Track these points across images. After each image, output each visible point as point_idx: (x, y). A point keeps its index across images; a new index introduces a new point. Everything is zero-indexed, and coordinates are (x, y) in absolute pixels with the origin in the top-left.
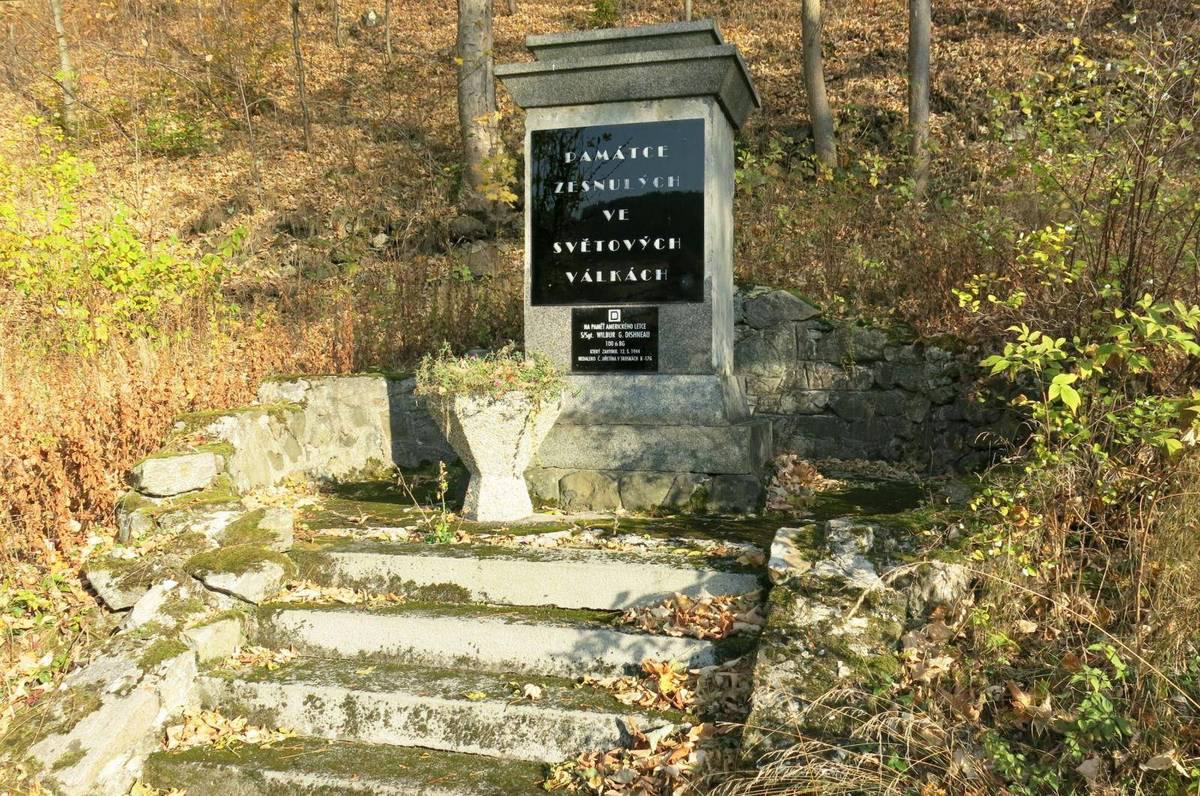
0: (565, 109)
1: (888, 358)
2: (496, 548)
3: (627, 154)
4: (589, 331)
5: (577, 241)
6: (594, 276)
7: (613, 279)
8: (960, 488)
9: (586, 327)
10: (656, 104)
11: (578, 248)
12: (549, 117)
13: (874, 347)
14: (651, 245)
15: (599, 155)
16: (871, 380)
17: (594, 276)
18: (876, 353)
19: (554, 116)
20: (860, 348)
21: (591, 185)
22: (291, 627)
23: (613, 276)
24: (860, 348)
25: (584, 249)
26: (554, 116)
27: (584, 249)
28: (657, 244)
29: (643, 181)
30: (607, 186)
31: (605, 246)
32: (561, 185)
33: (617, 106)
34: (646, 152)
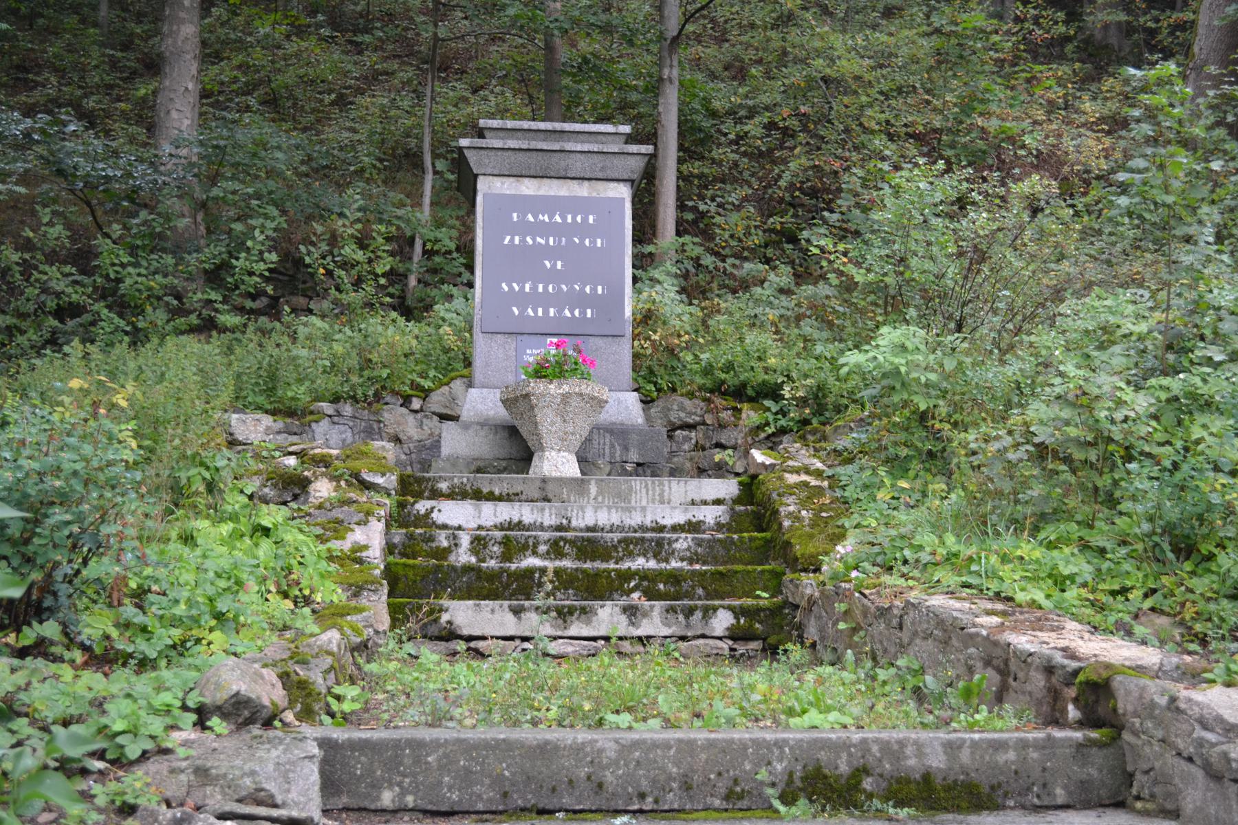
0: (512, 179)
1: (709, 422)
2: (355, 608)
3: (564, 218)
4: (531, 355)
5: (522, 283)
6: (535, 312)
7: (552, 314)
8: (808, 241)
9: (529, 352)
10: (586, 183)
11: (522, 288)
12: (499, 184)
13: (695, 414)
14: (583, 290)
15: (541, 217)
16: (693, 441)
17: (535, 312)
18: (698, 419)
19: (503, 184)
20: (682, 415)
21: (534, 240)
22: (423, 512)
23: (552, 312)
24: (682, 415)
25: (527, 290)
26: (503, 184)
27: (527, 290)
28: (588, 289)
29: (577, 240)
30: (547, 241)
31: (545, 288)
32: (508, 238)
33: (555, 181)
34: (579, 219)
